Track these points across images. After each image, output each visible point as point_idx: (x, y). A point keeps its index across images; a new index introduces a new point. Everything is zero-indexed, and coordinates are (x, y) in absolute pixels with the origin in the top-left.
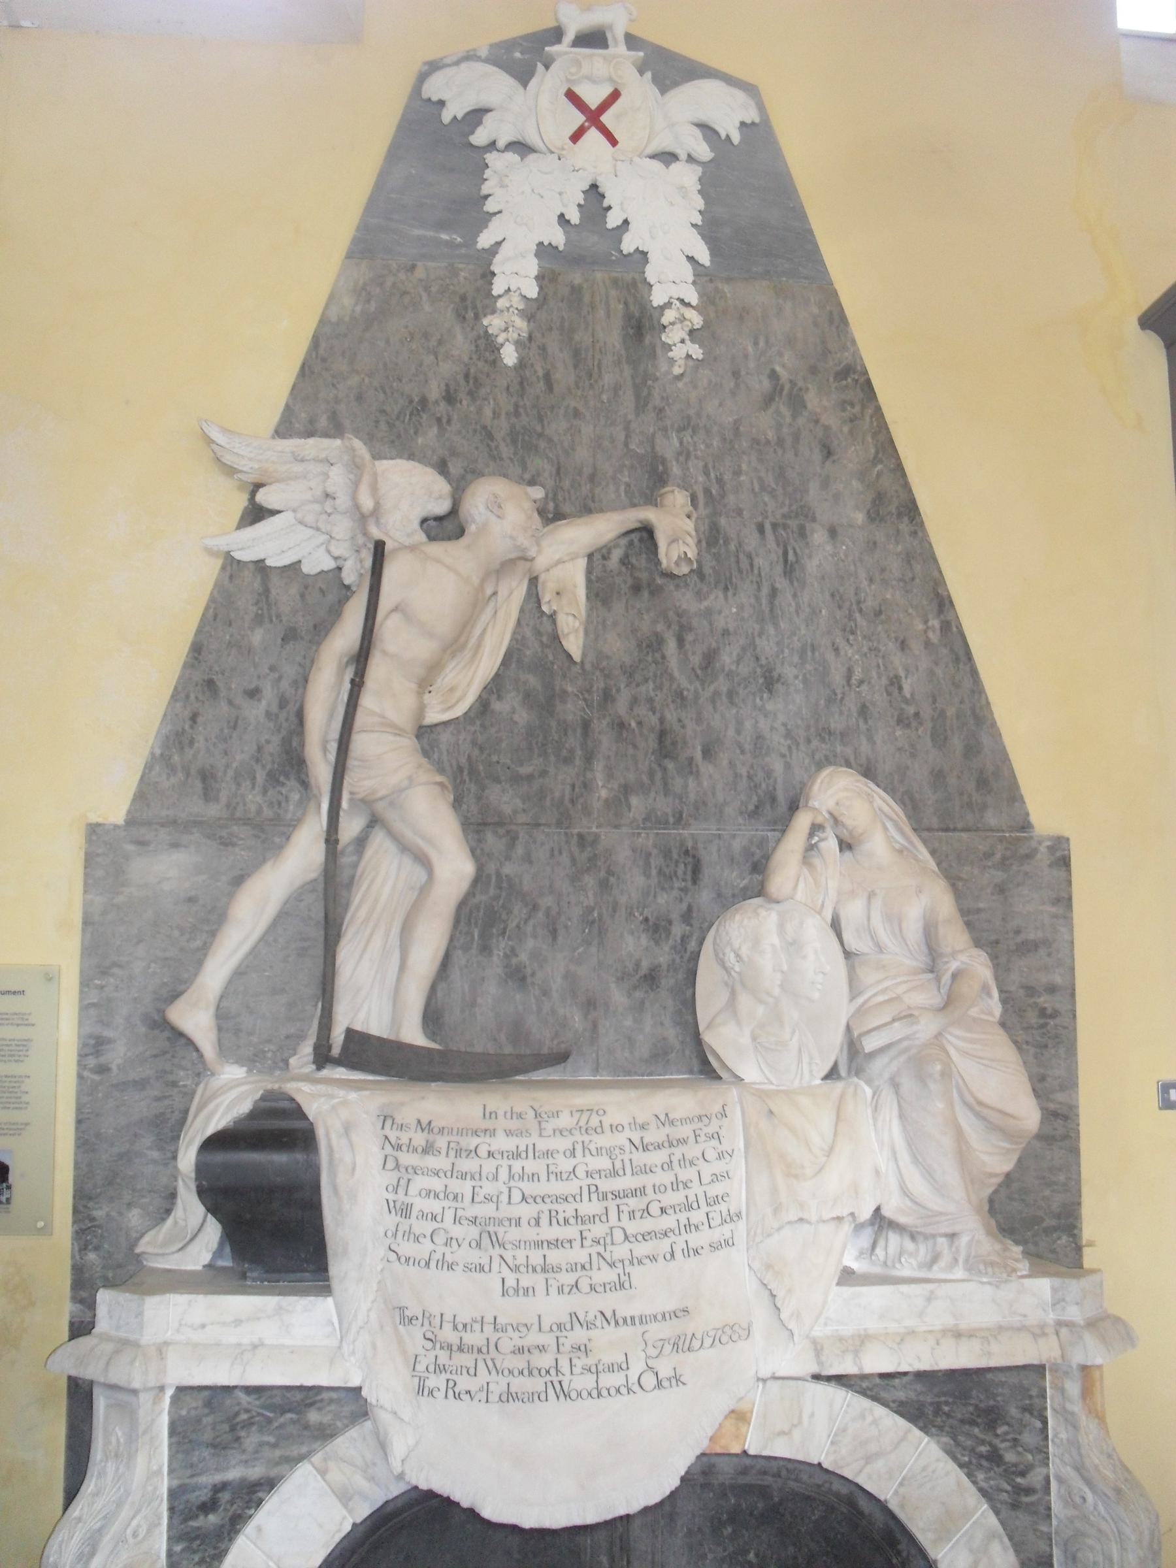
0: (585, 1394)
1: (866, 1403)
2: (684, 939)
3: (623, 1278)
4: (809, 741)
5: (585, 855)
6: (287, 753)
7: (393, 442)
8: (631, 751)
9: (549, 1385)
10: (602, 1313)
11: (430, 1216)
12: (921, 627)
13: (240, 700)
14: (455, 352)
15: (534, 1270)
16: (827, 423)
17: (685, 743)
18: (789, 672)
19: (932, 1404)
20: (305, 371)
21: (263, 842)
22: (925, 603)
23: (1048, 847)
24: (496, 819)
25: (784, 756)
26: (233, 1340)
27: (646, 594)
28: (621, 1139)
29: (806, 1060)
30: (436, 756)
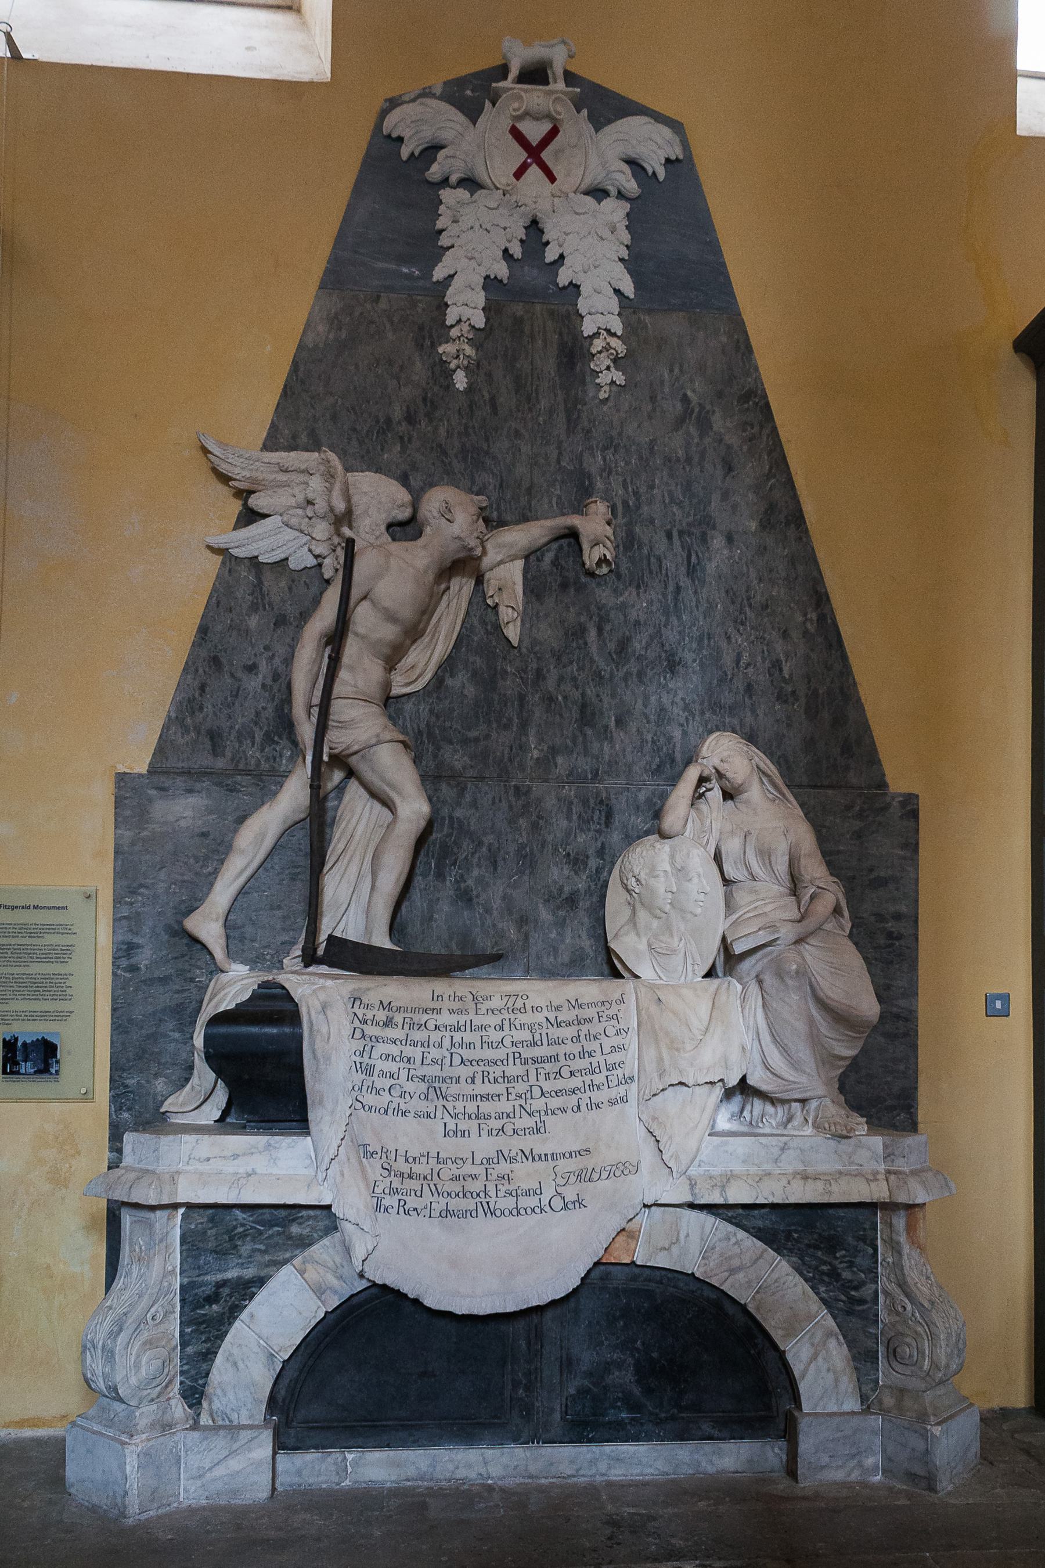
0: (507, 1212)
1: (731, 1228)
2: (599, 871)
3: (539, 1125)
4: (702, 713)
5: (520, 803)
6: (279, 717)
7: (363, 457)
8: (557, 718)
9: (479, 1205)
10: (522, 1151)
11: (388, 1074)
12: (801, 619)
13: (240, 674)
14: (415, 378)
15: (470, 1117)
16: (729, 442)
17: (602, 713)
18: (688, 656)
19: (783, 1231)
20: (287, 392)
21: (262, 789)
22: (805, 598)
23: (900, 802)
24: (449, 773)
25: (682, 725)
26: (231, 1170)
27: (572, 591)
28: (540, 1017)
29: (689, 961)
30: (400, 722)
